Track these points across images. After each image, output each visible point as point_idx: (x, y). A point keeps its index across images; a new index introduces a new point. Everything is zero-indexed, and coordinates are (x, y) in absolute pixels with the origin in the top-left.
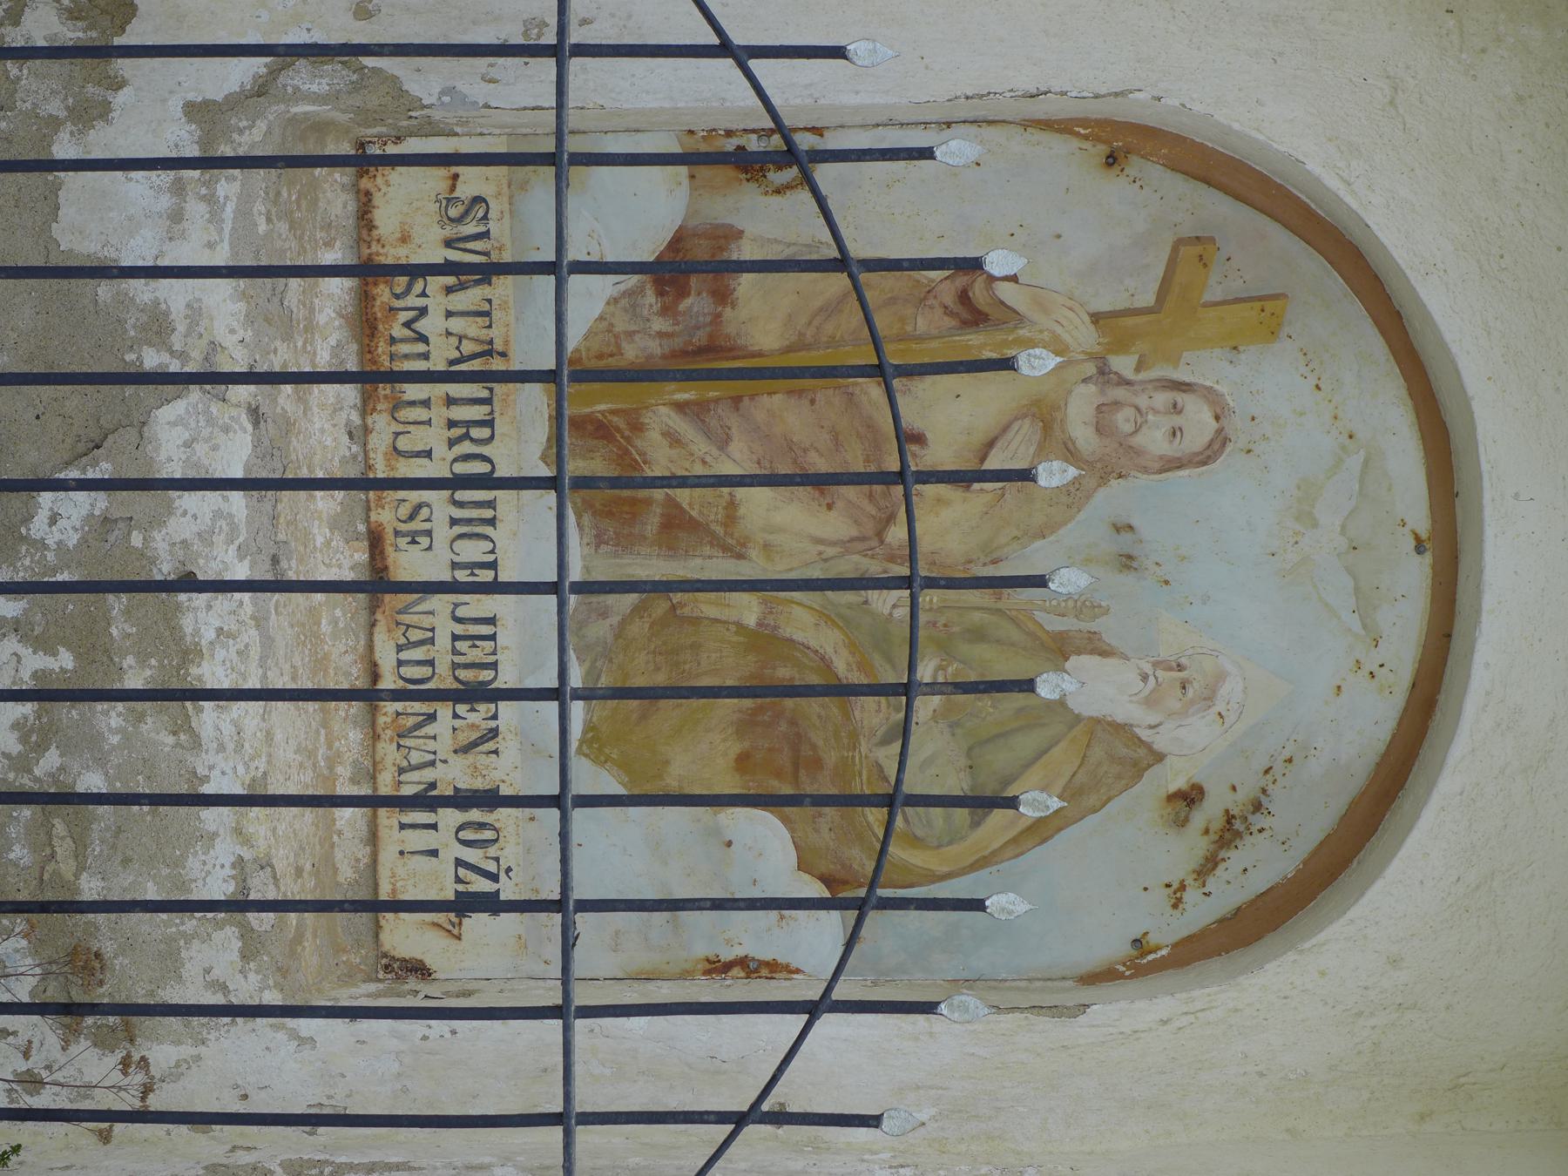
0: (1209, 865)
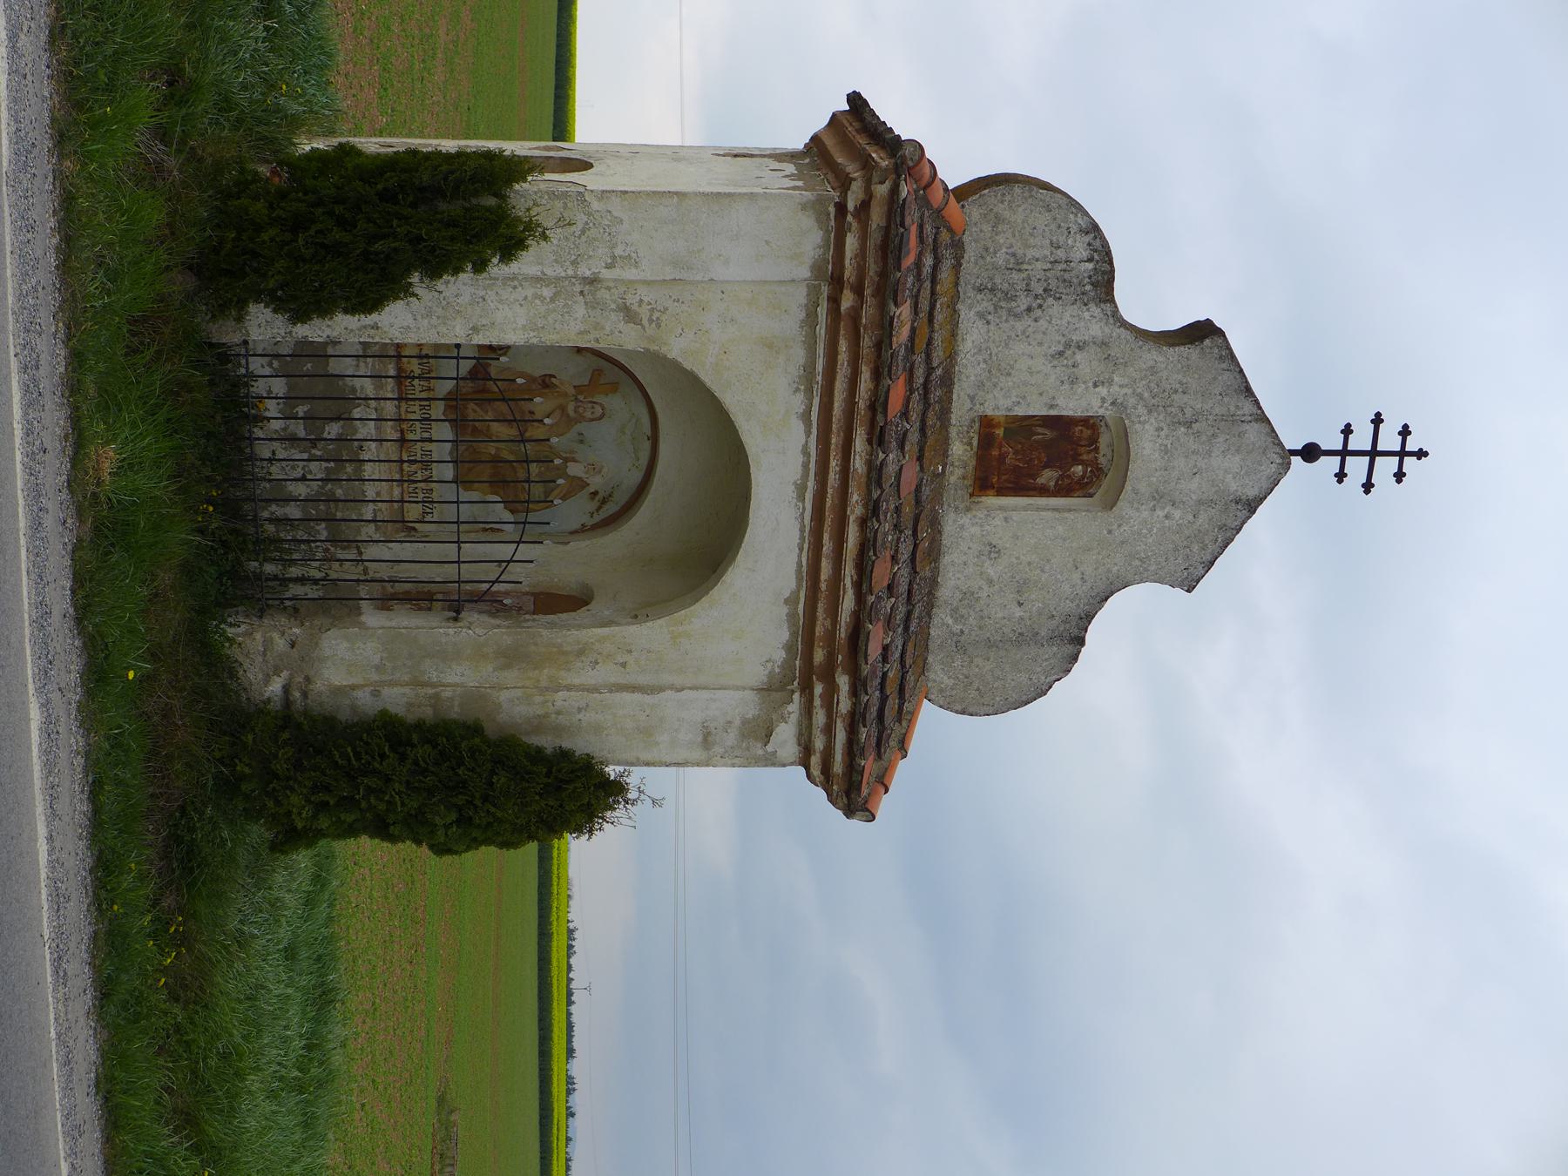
0: (598, 510)
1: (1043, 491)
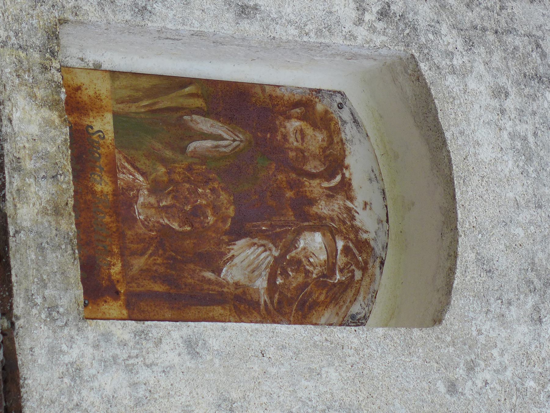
1: (240, 305)
